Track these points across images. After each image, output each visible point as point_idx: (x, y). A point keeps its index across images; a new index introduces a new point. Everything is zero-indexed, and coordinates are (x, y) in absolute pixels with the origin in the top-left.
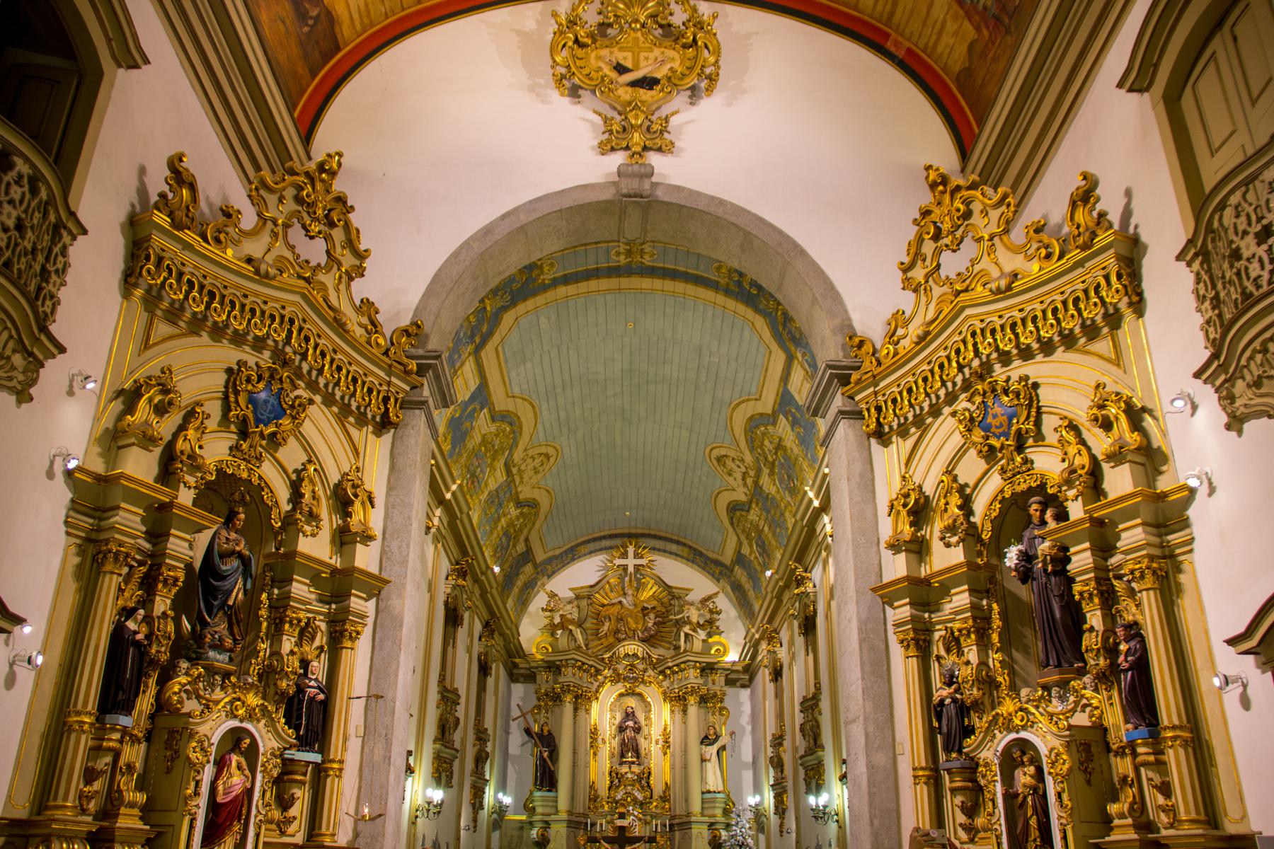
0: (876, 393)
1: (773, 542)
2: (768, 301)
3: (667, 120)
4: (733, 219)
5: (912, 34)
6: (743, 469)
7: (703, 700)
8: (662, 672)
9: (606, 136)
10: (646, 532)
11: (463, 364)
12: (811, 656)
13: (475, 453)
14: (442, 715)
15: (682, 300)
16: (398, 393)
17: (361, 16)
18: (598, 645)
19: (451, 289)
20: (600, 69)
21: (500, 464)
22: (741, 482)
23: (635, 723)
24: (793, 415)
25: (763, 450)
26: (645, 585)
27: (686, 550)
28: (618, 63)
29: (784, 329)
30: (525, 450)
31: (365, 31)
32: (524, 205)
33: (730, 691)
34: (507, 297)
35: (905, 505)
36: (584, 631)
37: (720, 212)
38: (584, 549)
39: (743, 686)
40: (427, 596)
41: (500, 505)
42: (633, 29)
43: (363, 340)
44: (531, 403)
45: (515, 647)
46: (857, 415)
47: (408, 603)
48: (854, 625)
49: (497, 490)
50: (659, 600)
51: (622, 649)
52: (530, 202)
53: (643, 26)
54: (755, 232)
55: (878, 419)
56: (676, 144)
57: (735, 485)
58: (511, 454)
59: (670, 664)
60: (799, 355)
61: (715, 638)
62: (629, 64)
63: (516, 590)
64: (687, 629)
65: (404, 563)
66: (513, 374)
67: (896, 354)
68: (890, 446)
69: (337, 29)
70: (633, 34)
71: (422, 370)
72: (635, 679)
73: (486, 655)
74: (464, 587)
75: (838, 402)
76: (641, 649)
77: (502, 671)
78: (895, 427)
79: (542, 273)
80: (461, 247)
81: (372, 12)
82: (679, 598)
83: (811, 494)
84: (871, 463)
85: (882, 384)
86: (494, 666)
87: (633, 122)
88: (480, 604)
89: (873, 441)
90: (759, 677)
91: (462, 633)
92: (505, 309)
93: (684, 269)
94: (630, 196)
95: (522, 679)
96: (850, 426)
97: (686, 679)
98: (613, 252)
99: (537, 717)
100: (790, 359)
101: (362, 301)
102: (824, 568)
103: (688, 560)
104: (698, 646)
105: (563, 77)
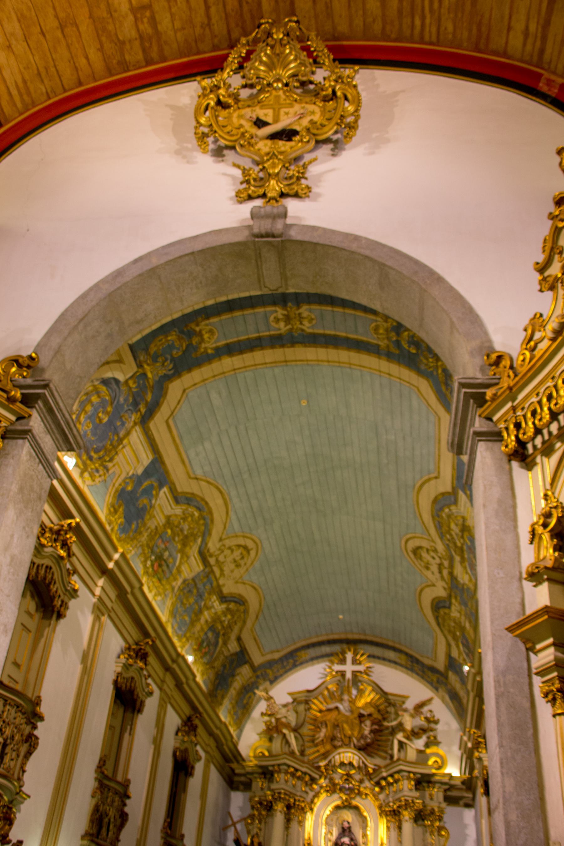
0: (514, 409)
2: (427, 359)
3: (305, 167)
4: (367, 252)
6: (438, 561)
8: (378, 784)
9: (245, 186)
10: (363, 637)
11: (128, 433)
13: (158, 534)
15: (348, 370)
18: (314, 753)
19: (76, 327)
20: (241, 126)
21: (193, 551)
22: (438, 575)
23: (352, 839)
25: (451, 535)
27: (403, 657)
30: (221, 540)
31: (28, 110)
32: (157, 250)
35: (545, 525)
37: (354, 247)
40: (79, 668)
41: (200, 596)
49: (193, 579)
51: (337, 757)
52: (163, 247)
54: (389, 263)
58: (204, 543)
59: (384, 774)
62: (269, 119)
63: (233, 692)
64: (400, 736)
66: (192, 454)
70: (274, 93)
71: (28, 401)
72: (351, 790)
73: (186, 750)
76: (356, 758)
78: (539, 446)
79: (202, 340)
80: (90, 289)
81: (32, 90)
82: (394, 705)
84: (512, 488)
85: (521, 397)
89: (515, 465)
92: (169, 378)
94: (262, 236)
95: (241, 787)
96: (487, 449)
98: (272, 318)
99: (250, 827)
103: (406, 668)
104: (411, 755)
105: (205, 135)
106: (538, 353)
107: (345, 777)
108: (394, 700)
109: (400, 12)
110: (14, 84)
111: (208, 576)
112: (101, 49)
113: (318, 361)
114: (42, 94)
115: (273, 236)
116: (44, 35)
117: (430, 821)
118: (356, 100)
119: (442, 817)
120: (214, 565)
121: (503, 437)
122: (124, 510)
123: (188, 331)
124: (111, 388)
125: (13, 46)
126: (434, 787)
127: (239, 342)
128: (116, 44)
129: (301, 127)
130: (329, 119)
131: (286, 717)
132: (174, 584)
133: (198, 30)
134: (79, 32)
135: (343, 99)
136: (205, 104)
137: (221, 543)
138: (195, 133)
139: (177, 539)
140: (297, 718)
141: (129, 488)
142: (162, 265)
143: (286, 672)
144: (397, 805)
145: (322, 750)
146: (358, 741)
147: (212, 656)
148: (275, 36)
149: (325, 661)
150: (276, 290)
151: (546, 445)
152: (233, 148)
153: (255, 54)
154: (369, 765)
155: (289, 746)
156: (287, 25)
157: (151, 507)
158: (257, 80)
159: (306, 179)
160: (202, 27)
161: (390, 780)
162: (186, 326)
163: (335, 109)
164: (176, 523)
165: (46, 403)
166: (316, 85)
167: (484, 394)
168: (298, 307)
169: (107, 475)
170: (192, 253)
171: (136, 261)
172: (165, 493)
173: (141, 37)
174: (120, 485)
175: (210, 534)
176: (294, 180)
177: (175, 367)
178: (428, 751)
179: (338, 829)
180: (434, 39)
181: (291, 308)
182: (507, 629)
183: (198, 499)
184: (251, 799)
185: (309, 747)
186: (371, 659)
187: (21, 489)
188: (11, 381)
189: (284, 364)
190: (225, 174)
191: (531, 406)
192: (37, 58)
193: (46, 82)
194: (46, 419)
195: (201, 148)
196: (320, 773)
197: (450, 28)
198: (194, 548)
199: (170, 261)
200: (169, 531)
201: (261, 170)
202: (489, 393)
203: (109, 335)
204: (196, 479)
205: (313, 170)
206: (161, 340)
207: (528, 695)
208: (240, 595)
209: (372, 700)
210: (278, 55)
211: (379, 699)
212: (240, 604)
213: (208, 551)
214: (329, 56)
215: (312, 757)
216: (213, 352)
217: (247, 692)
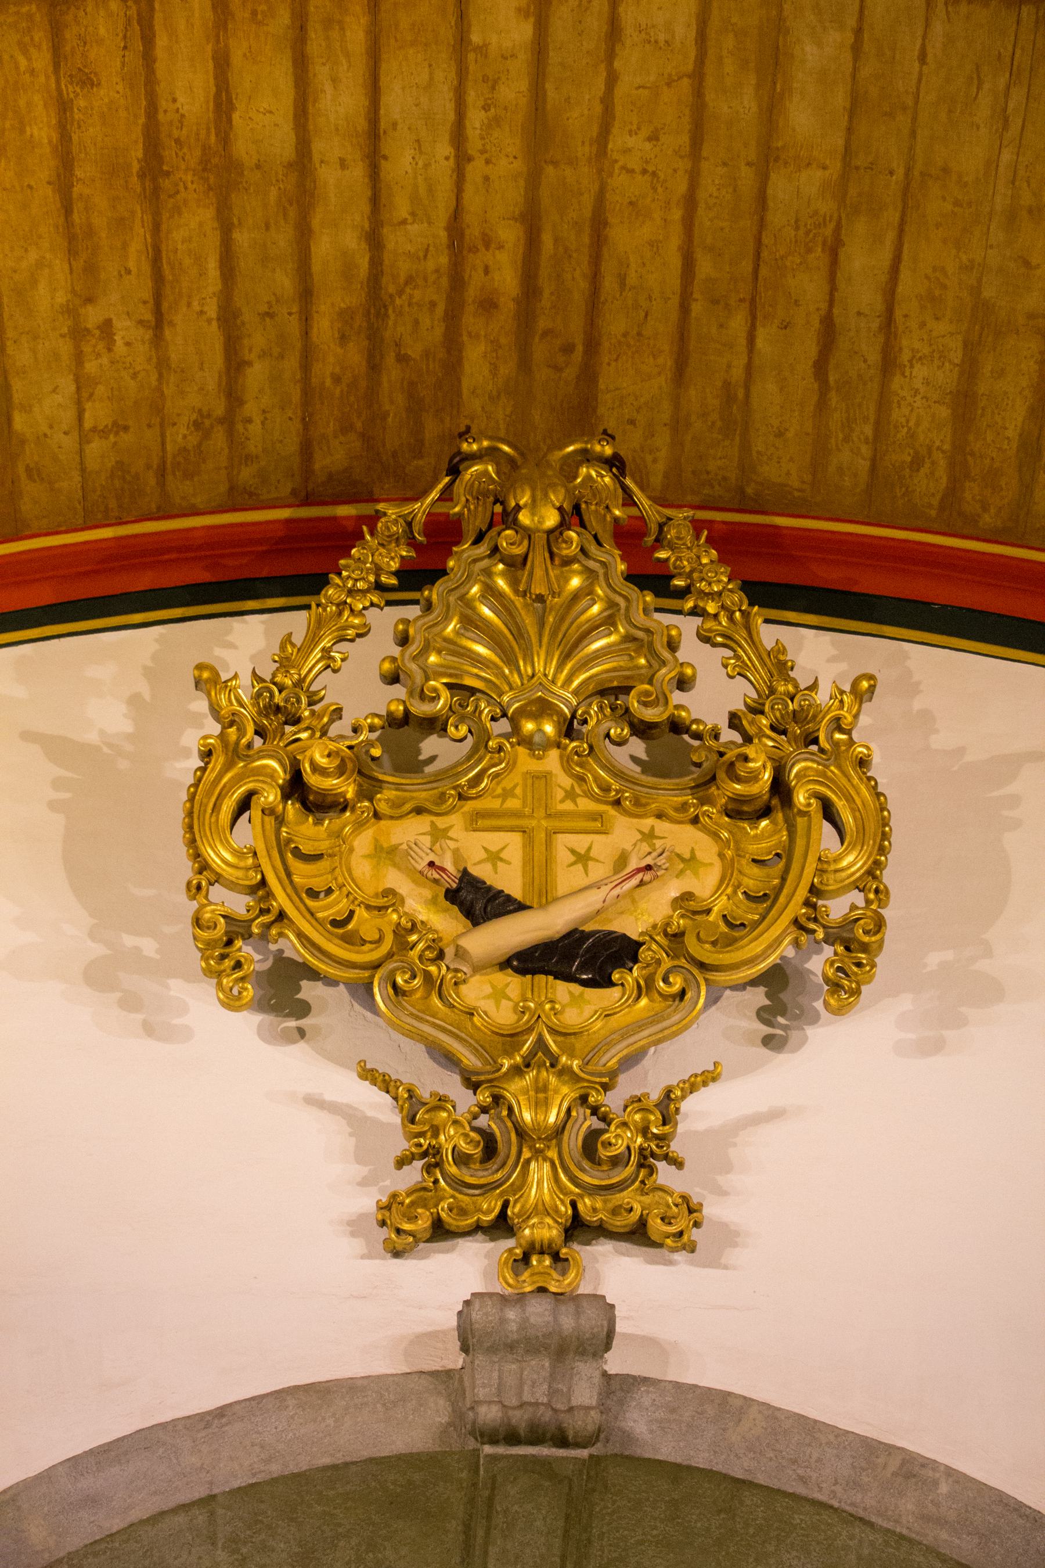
32: (47, 1476)
42: (527, 742)
53: (569, 729)
56: (710, 1211)
115: (562, 1441)
118: (871, 826)
133: (180, 435)
138: (197, 922)
148: (524, 518)
160: (197, 425)
163: (785, 855)
190: (315, 1102)
210: (540, 599)
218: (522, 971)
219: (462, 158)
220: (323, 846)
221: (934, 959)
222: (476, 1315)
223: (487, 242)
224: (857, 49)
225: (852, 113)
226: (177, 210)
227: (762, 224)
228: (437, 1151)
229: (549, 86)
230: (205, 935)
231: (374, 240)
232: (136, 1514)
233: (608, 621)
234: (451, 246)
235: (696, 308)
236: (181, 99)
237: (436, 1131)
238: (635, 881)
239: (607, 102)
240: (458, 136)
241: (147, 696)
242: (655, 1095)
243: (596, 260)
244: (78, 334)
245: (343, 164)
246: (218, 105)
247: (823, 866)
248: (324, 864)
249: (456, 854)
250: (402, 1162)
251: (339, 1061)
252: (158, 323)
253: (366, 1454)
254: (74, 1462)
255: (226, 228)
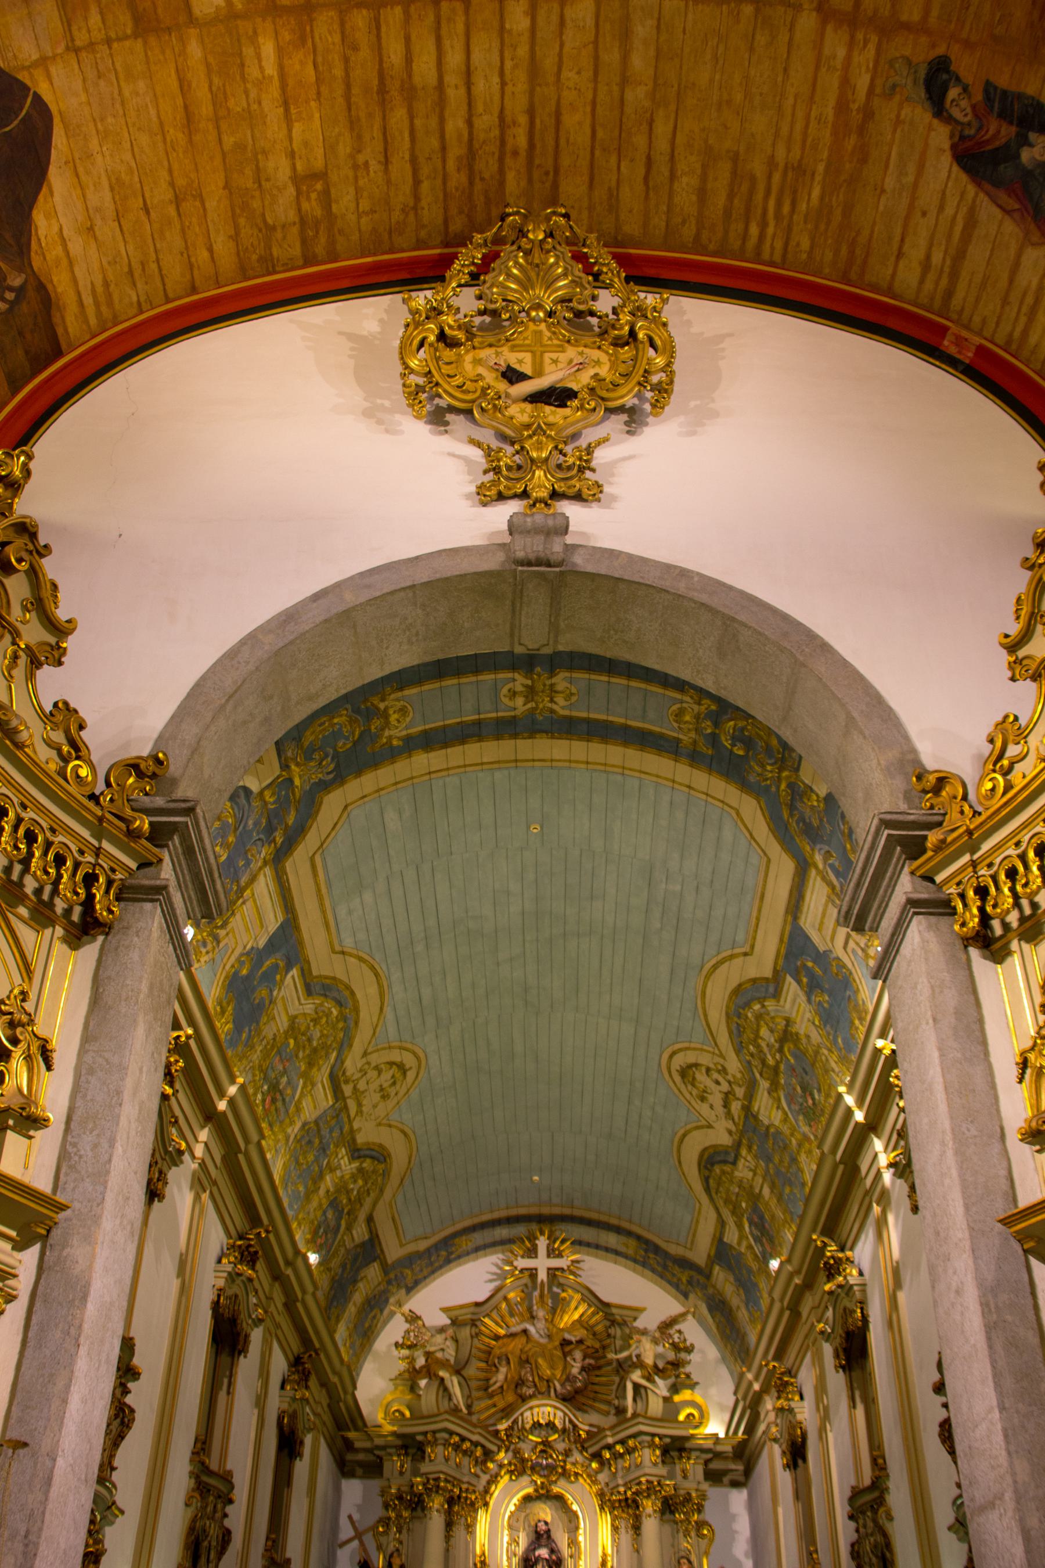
0: (974, 864)
1: (780, 1214)
2: (763, 766)
3: (589, 450)
4: (704, 598)
5: (984, 321)
6: (725, 1087)
7: (668, 1507)
8: (597, 1456)
9: (491, 476)
10: (567, 1211)
11: (253, 879)
12: (860, 1412)
13: (276, 1048)
14: (194, 1520)
15: (619, 778)
16: (113, 870)
17: (97, 304)
18: (488, 1408)
19: (222, 707)
20: (480, 378)
21: (322, 1075)
22: (720, 1110)
23: (552, 1551)
24: (812, 976)
25: (758, 1047)
26: (566, 1302)
27: (632, 1243)
28: (509, 367)
29: (791, 815)
30: (365, 1054)
32: (352, 578)
33: (714, 1492)
34: (329, 765)
36: (465, 1382)
37: (681, 588)
38: (465, 1243)
39: (735, 1484)
40: (176, 1283)
41: (323, 1149)
42: (533, 320)
43: (52, 767)
44: (373, 968)
45: (348, 1408)
46: (942, 908)
47: (103, 1255)
48: (971, 1297)
49: (316, 1122)
50: (590, 1328)
51: (528, 1414)
53: (550, 314)
54: (742, 617)
55: (982, 910)
56: (606, 489)
57: (712, 1118)
58: (340, 1060)
59: (610, 1440)
60: (818, 858)
61: (686, 1395)
62: (527, 369)
63: (351, 1309)
64: (636, 1376)
65: (101, 1176)
66: (342, 911)
67: (1008, 787)
68: (1009, 960)
69: (56, 319)
70: (532, 326)
71: (158, 835)
72: (551, 1468)
73: (293, 1416)
74: (250, 1280)
75: (905, 886)
77: (324, 1454)
78: (1015, 924)
79: (387, 724)
80: (243, 642)
81: (116, 297)
83: (850, 1100)
84: (975, 992)
85: (986, 847)
86: (308, 1440)
87: (535, 455)
88: (283, 1320)
89: (974, 953)
90: (763, 1466)
91: (247, 1366)
92: (325, 786)
93: (622, 721)
94: (529, 564)
95: (359, 1471)
96: (929, 927)
97: (637, 1466)
98: (505, 691)
99: (383, 1540)
100: (803, 868)
101: (56, 705)
102: (879, 1236)
103: (635, 1261)
104: (655, 1406)
105: (419, 389)
106: (1017, 778)
107: (540, 1448)
108: (621, 1316)
109: (728, 213)
110: (89, 287)
111: (338, 1116)
112: (236, 237)
113: (570, 761)
114: (131, 304)
115: (549, 565)
116: (148, 212)
117: (684, 1514)
118: (668, 347)
119: (702, 1506)
120: (349, 1097)
121: (954, 908)
122: (234, 1009)
123: (367, 709)
124: (237, 804)
125: (96, 229)
126: (689, 1458)
127: (444, 727)
128: (260, 230)
129: (580, 386)
130: (626, 376)
131: (443, 1350)
132: (289, 1130)
133: (397, 215)
134: (205, 210)
135: (647, 344)
136: (420, 337)
137: (364, 1060)
138: (404, 385)
139: (301, 1055)
140: (457, 1351)
141: (245, 972)
142: (361, 604)
143: (433, 1272)
144: (634, 1490)
145: (501, 1404)
146: (563, 1385)
147: (329, 1251)
148: (531, 236)
149: (496, 1253)
150: (538, 650)
151: (1027, 925)
152: (468, 413)
153: (498, 262)
154: (580, 1425)
155: (450, 1399)
156: (550, 220)
157: (271, 1002)
158: (504, 304)
159: (593, 470)
160: (403, 210)
161: (620, 1448)
162: (366, 700)
163: (635, 359)
164: (303, 1028)
165: (186, 840)
166: (600, 317)
167: (925, 837)
168: (552, 674)
169: (217, 950)
170: (412, 587)
171: (316, 597)
172: (293, 977)
173: (303, 222)
174: (233, 966)
175: (351, 1046)
176: (575, 471)
177: (337, 767)
178: (677, 1398)
179: (527, 1535)
180: (777, 258)
181: (539, 675)
182: (1000, 1221)
183: (341, 987)
184: (383, 1492)
185: (479, 1399)
186: (577, 1247)
187: (151, 988)
188: (128, 800)
189: (513, 764)
191: (1005, 862)
192: (131, 248)
193: (140, 285)
194: (180, 865)
195: (414, 410)
196: (499, 1443)
197: (806, 244)
198: (323, 1070)
199: (376, 598)
200: (292, 1041)
201: (517, 452)
202: (933, 837)
203: (267, 720)
204: (343, 953)
205: (602, 456)
206: (324, 723)
207: (1036, 1326)
208: (381, 1146)
209: (581, 1316)
210: (537, 266)
211: (593, 1314)
212: (379, 1161)
213: (344, 1073)
214: (618, 272)
215: (483, 1417)
216: (401, 743)
217: (372, 1309)
218: (531, 402)
219: (503, 84)
220: (453, 359)
221: (692, 404)
222: (515, 520)
223: (514, 123)
224: (658, 27)
225: (657, 58)
226: (392, 109)
227: (622, 112)
228: (499, 467)
229: (537, 48)
230: (408, 390)
231: (470, 123)
232: (385, 591)
233: (565, 275)
234: (500, 125)
235: (597, 153)
236: (392, 56)
237: (499, 460)
238: (576, 368)
239: (560, 55)
240: (502, 74)
241: (386, 318)
242: (584, 446)
243: (557, 130)
244: (355, 167)
245: (456, 87)
246: (407, 59)
247: (650, 362)
248: (453, 365)
249: (505, 361)
250: (485, 472)
251: (460, 440)
252: (387, 162)
253: (473, 570)
254: (361, 574)
255: (412, 118)
